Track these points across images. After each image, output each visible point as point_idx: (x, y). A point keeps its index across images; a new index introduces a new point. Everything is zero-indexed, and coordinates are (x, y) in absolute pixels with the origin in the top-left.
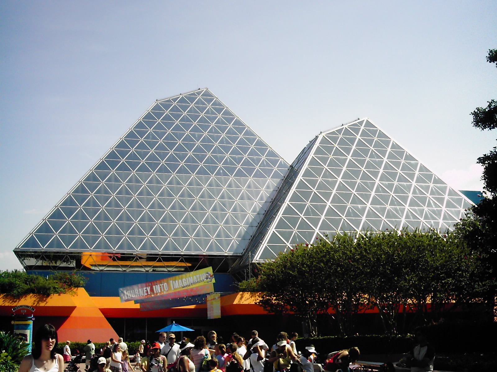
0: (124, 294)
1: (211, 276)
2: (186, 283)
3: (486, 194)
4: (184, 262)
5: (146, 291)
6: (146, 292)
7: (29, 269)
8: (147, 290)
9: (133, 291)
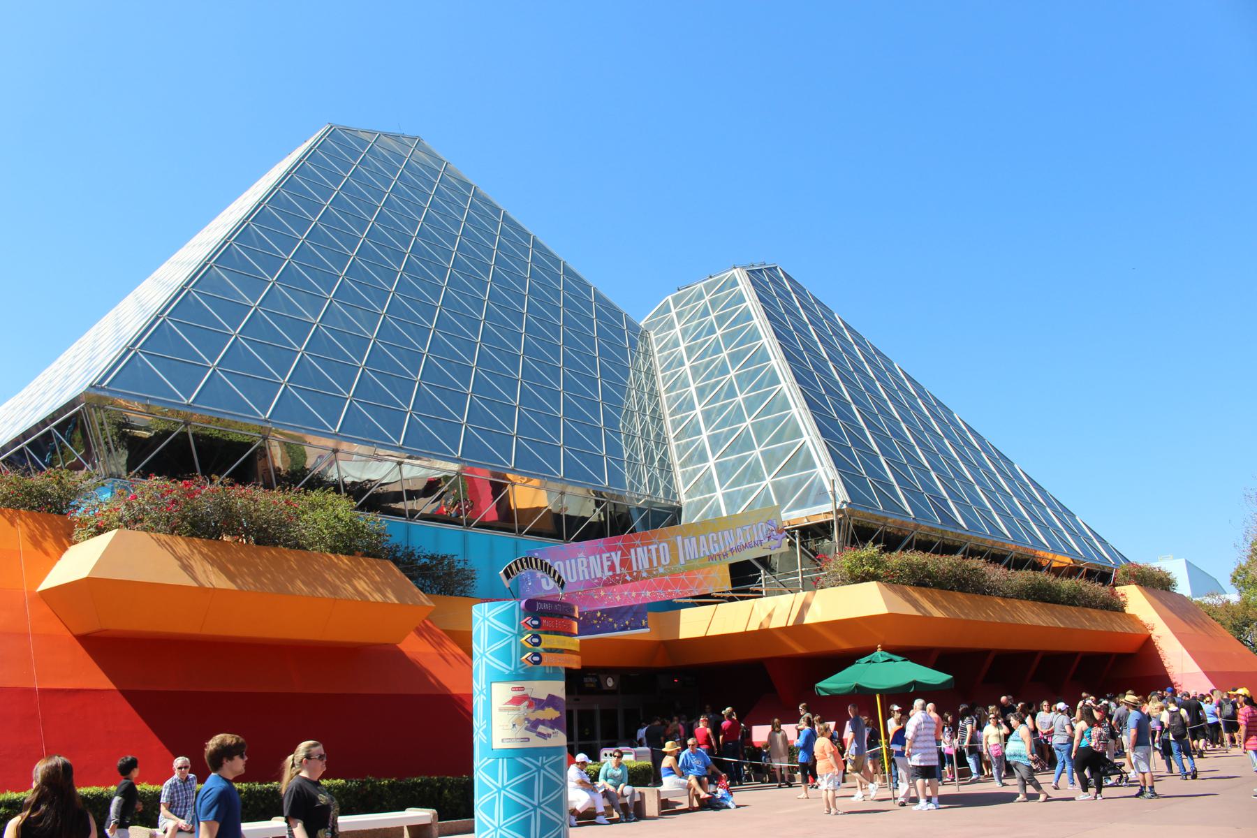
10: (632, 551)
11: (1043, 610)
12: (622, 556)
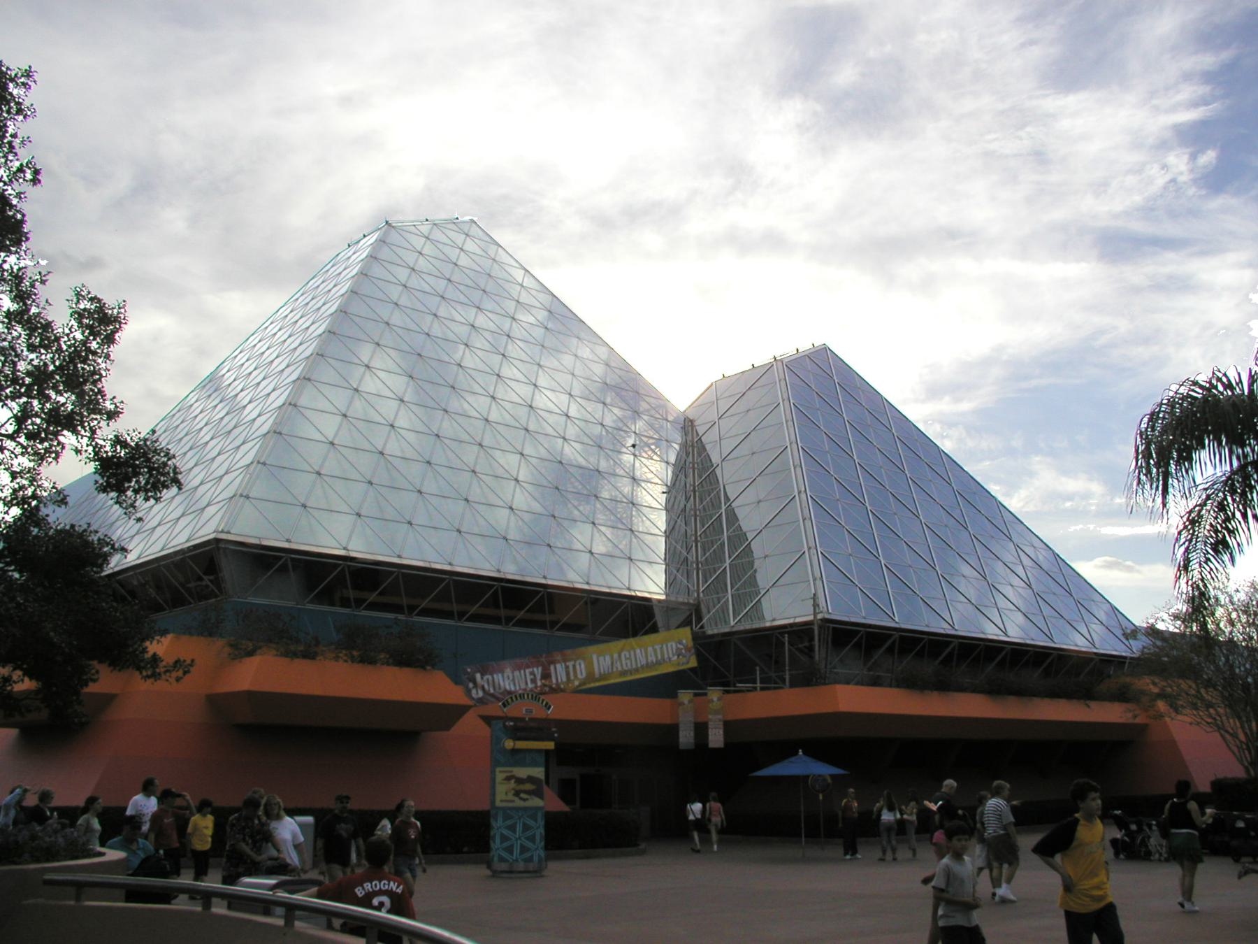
0: (474, 682)
1: (687, 649)
2: (628, 662)
4: (755, 571)
5: (532, 677)
8: (535, 675)
10: (552, 668)
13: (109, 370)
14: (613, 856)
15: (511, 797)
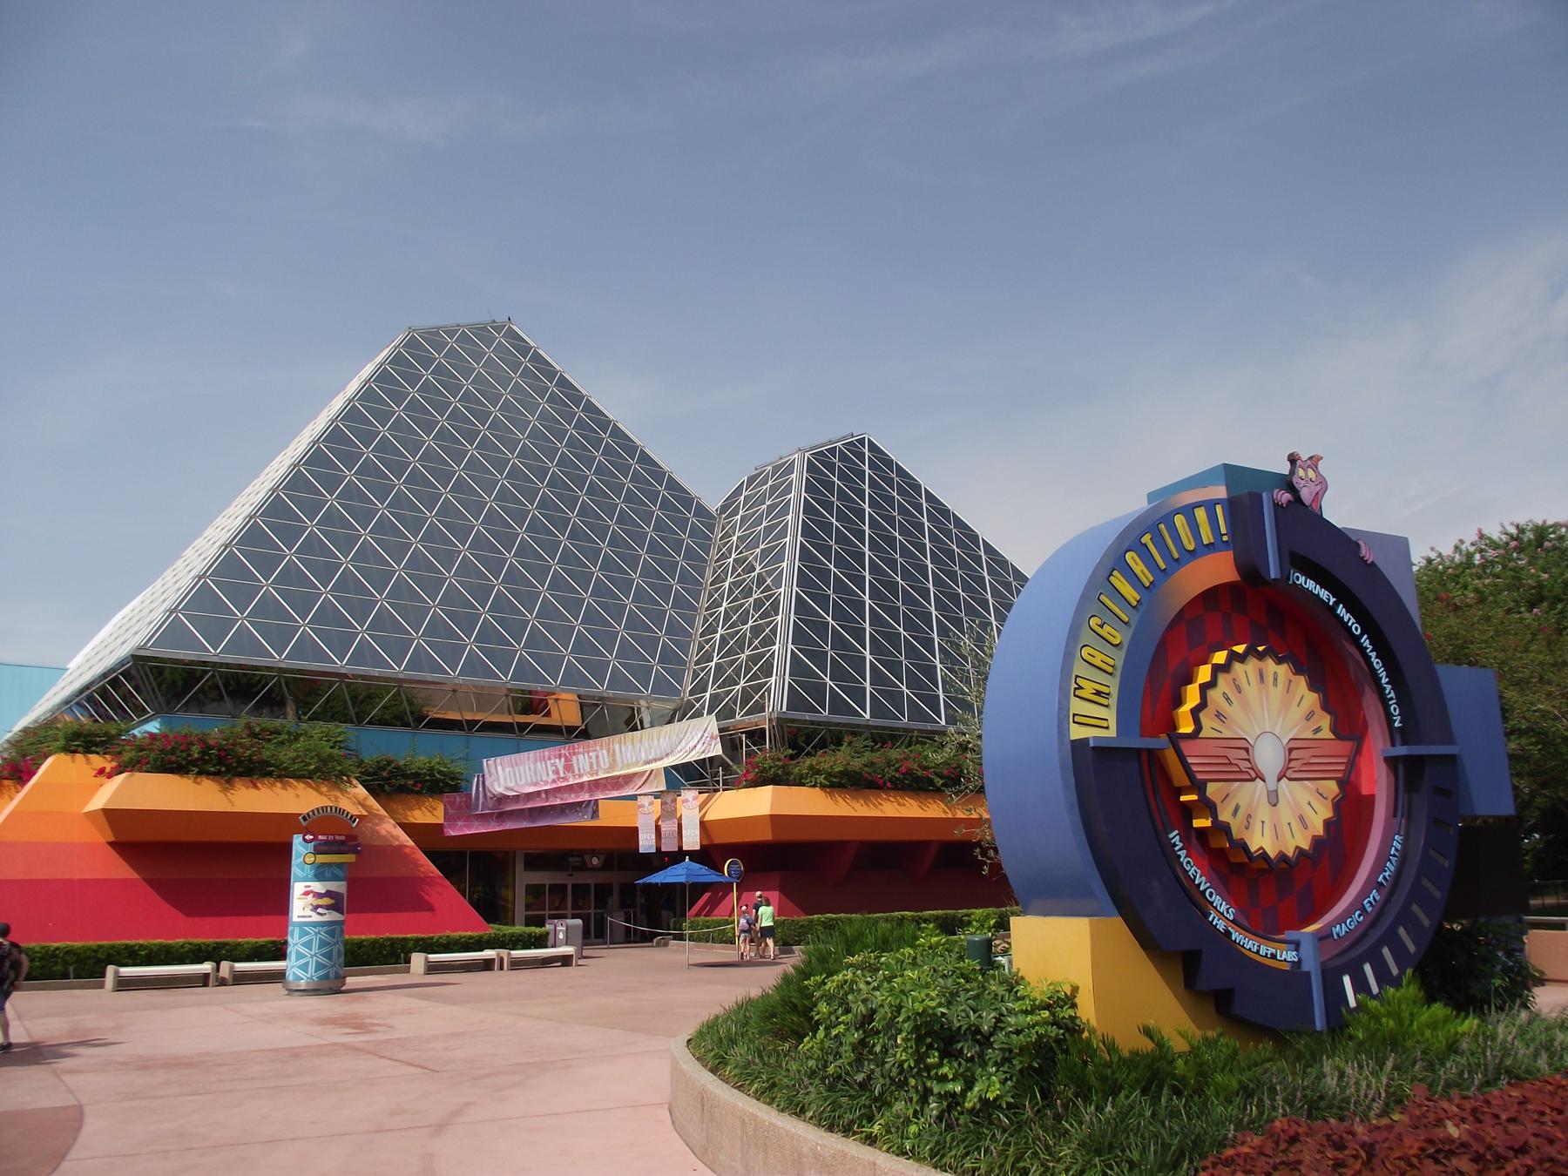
3: (1275, 673)
6: (553, 771)
7: (165, 709)
8: (556, 766)
9: (521, 767)
10: (574, 758)
11: (935, 802)
12: (565, 762)
13: (1368, 1163)
14: (27, 1068)
15: (308, 912)
